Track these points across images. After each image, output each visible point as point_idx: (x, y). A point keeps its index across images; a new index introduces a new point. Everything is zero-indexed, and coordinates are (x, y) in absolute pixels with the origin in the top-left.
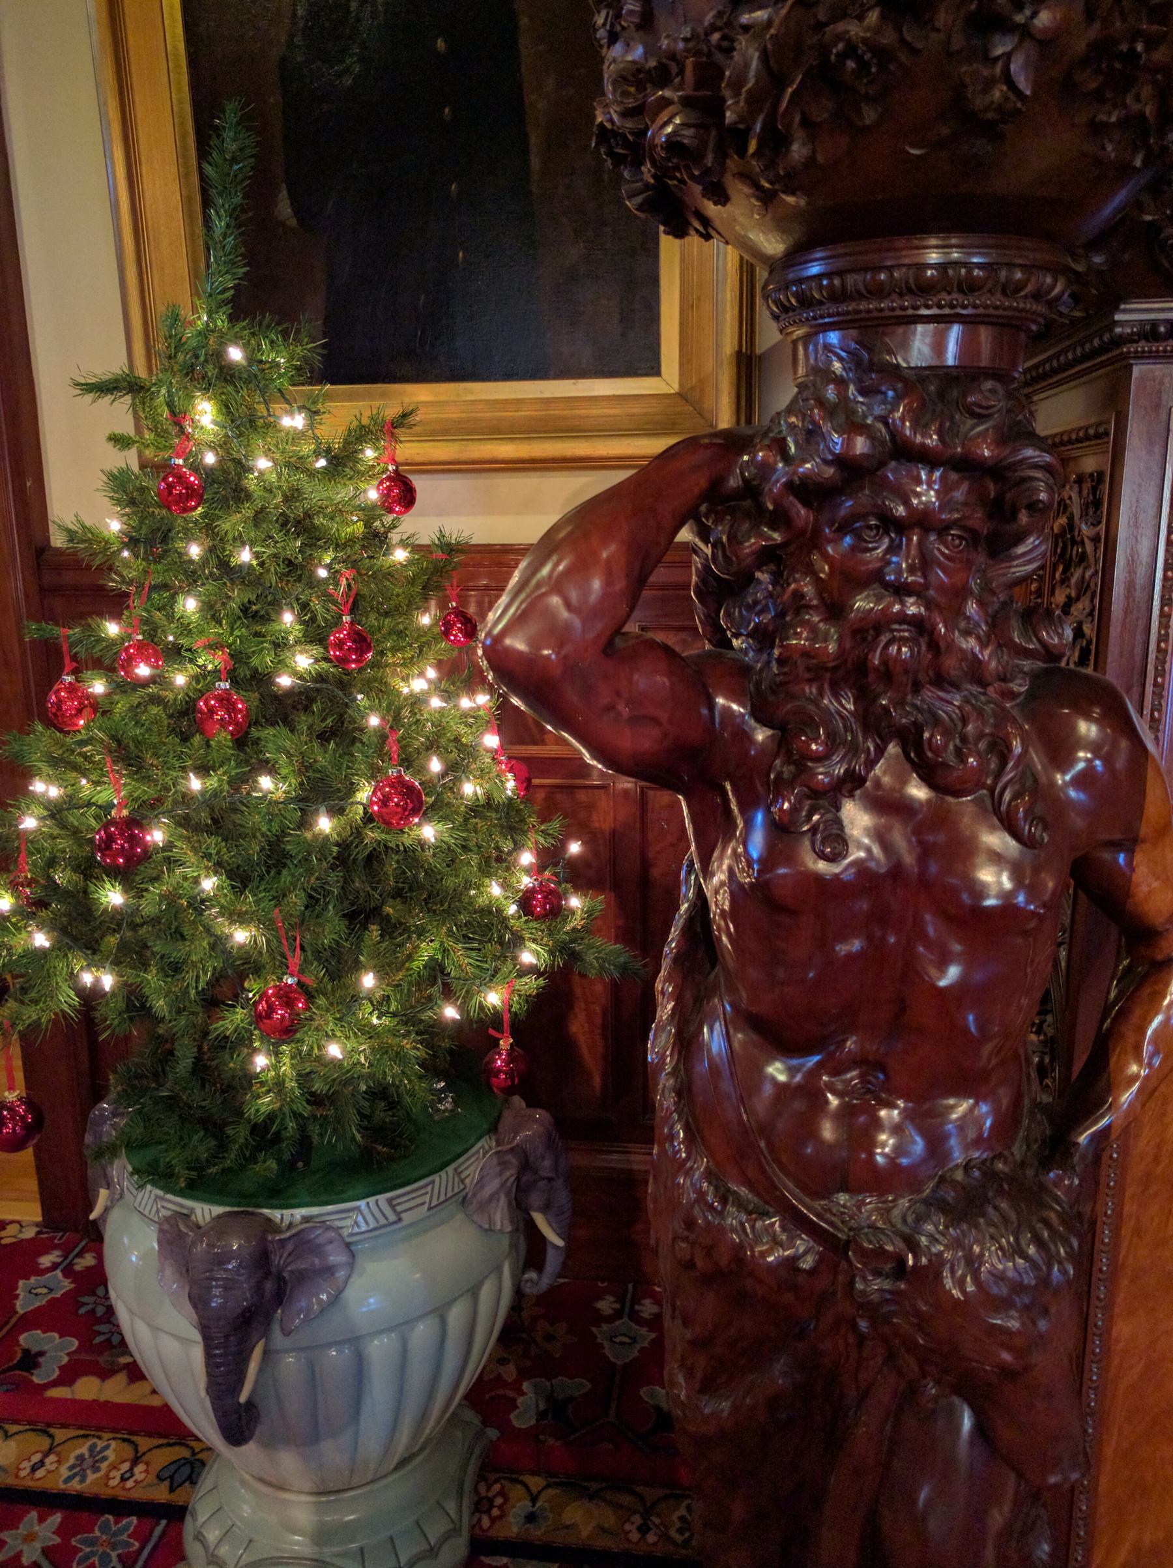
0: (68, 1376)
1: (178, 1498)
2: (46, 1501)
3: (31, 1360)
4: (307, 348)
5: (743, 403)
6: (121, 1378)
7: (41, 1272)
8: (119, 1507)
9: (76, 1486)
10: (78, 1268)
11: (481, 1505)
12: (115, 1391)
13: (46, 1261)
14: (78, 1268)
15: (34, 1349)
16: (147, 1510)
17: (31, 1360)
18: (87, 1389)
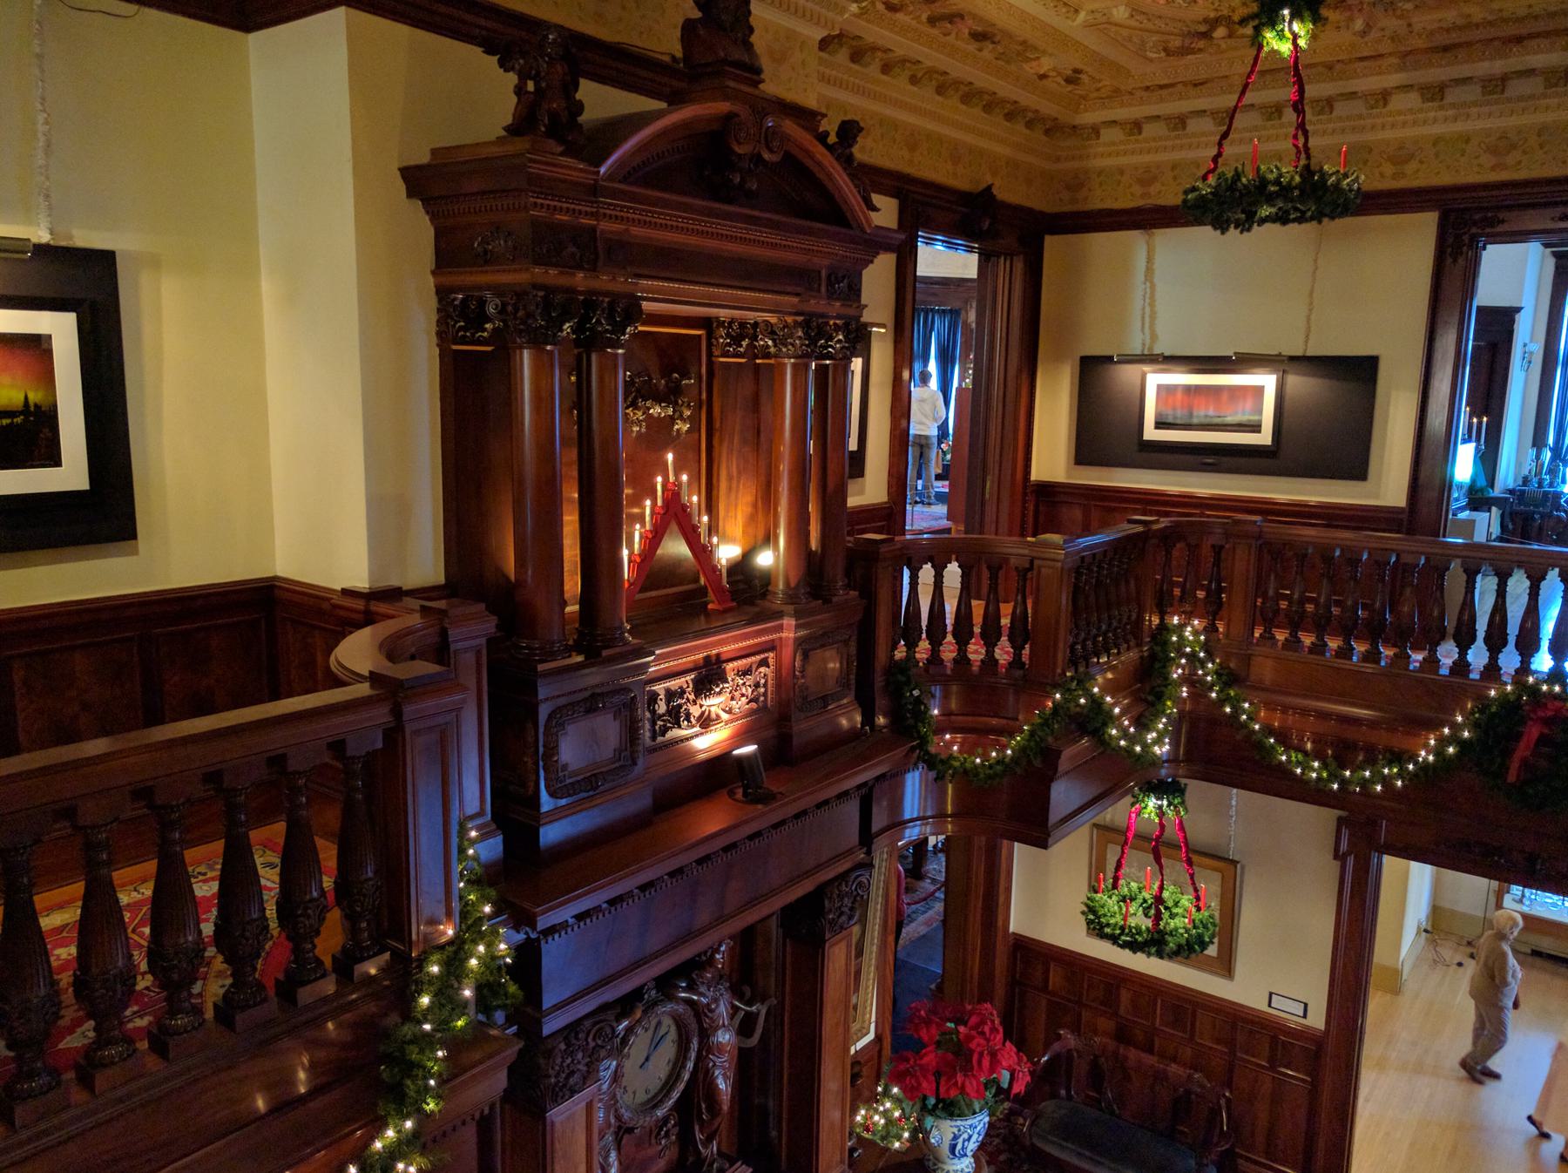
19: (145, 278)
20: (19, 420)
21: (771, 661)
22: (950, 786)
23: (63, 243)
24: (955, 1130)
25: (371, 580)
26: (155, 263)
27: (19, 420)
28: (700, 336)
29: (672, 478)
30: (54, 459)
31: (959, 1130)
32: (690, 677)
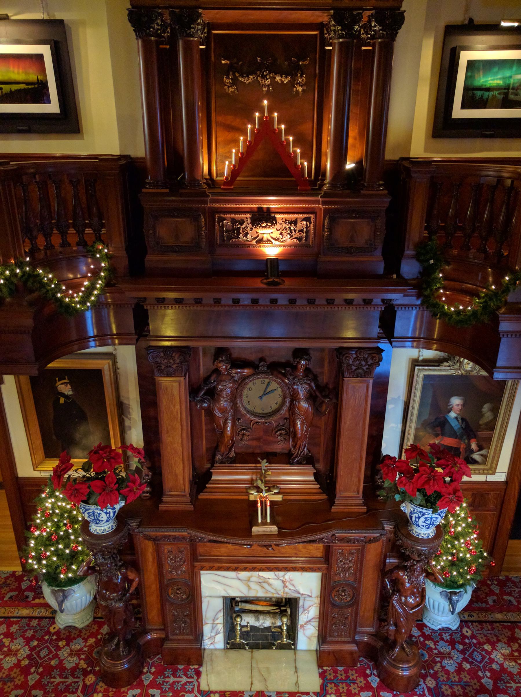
0: (34, 599)
1: (54, 616)
2: (35, 618)
3: (27, 597)
4: (149, 465)
5: (338, 415)
6: (42, 599)
7: (32, 674)
8: (46, 618)
9: (39, 615)
10: (39, 672)
11: (95, 613)
12: (41, 601)
13: (25, 579)
14: (39, 672)
15: (35, 695)
16: (50, 618)
17: (27, 597)
18: (37, 601)
19: (81, 30)
20: (36, 86)
21: (312, 220)
22: (438, 321)
23: (52, 18)
24: (412, 510)
25: (121, 151)
26: (83, 23)
27: (36, 86)
28: (316, 35)
29: (266, 114)
31: (414, 511)
32: (249, 216)
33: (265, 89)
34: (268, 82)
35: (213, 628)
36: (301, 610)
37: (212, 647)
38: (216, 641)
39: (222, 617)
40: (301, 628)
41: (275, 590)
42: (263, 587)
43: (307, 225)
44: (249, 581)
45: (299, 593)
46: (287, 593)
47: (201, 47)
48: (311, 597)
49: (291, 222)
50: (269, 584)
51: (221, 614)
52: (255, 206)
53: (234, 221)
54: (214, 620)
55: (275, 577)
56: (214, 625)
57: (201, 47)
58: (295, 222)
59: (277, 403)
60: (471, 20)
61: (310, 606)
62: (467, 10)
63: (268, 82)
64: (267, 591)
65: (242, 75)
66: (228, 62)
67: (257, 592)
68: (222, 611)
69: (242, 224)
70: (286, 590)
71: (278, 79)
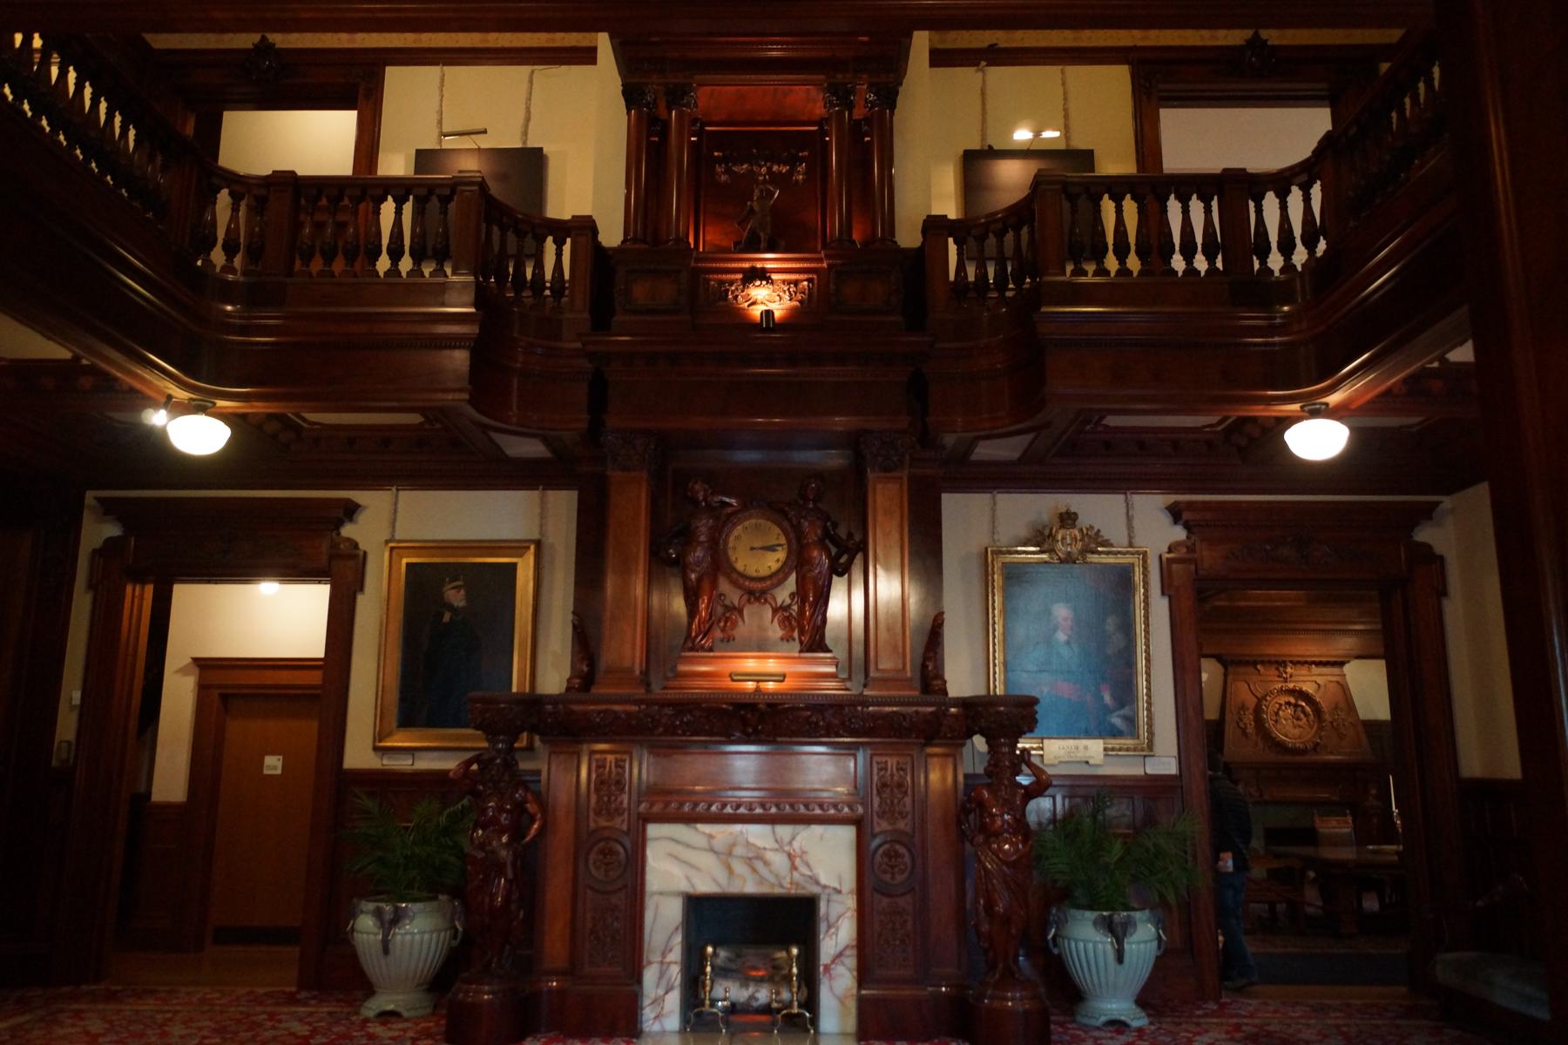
21: (816, 282)
30: (407, 564)
32: (740, 276)
33: (761, 178)
34: (764, 170)
35: (662, 975)
36: (823, 927)
37: (656, 1027)
38: (664, 1012)
39: (680, 945)
40: (824, 975)
41: (777, 876)
42: (754, 870)
43: (808, 286)
44: (730, 854)
45: (817, 883)
46: (797, 885)
47: (692, 139)
48: (839, 892)
49: (789, 283)
50: (766, 863)
51: (678, 939)
52: (747, 265)
53: (722, 282)
54: (664, 955)
55: (776, 846)
56: (665, 967)
57: (692, 139)
58: (796, 283)
59: (778, 560)
60: (990, 147)
61: (839, 917)
62: (983, 137)
63: (764, 170)
64: (762, 881)
65: (735, 165)
66: (721, 154)
67: (745, 881)
68: (680, 929)
69: (731, 285)
70: (796, 875)
71: (775, 168)
